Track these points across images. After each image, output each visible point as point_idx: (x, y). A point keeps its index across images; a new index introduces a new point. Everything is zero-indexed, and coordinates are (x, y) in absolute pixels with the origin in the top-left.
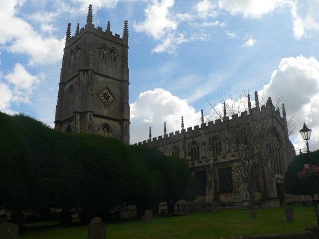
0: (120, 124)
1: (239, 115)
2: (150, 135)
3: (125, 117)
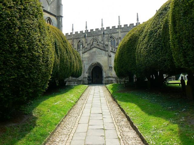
0: (57, 19)
1: (79, 33)
2: (73, 30)
3: (61, 15)
